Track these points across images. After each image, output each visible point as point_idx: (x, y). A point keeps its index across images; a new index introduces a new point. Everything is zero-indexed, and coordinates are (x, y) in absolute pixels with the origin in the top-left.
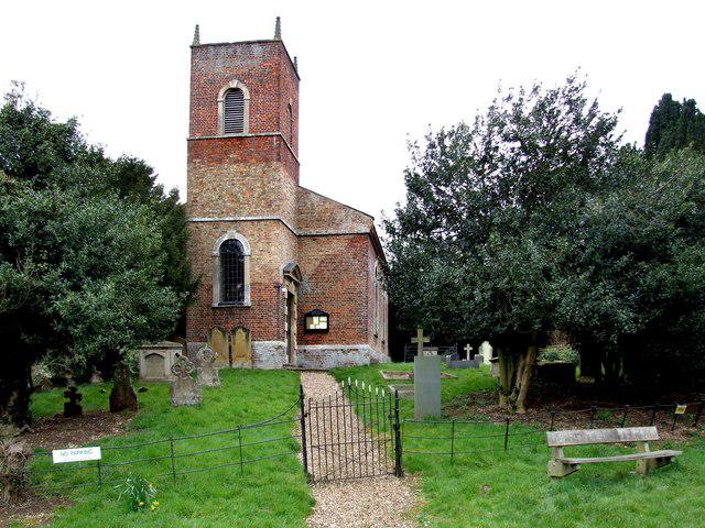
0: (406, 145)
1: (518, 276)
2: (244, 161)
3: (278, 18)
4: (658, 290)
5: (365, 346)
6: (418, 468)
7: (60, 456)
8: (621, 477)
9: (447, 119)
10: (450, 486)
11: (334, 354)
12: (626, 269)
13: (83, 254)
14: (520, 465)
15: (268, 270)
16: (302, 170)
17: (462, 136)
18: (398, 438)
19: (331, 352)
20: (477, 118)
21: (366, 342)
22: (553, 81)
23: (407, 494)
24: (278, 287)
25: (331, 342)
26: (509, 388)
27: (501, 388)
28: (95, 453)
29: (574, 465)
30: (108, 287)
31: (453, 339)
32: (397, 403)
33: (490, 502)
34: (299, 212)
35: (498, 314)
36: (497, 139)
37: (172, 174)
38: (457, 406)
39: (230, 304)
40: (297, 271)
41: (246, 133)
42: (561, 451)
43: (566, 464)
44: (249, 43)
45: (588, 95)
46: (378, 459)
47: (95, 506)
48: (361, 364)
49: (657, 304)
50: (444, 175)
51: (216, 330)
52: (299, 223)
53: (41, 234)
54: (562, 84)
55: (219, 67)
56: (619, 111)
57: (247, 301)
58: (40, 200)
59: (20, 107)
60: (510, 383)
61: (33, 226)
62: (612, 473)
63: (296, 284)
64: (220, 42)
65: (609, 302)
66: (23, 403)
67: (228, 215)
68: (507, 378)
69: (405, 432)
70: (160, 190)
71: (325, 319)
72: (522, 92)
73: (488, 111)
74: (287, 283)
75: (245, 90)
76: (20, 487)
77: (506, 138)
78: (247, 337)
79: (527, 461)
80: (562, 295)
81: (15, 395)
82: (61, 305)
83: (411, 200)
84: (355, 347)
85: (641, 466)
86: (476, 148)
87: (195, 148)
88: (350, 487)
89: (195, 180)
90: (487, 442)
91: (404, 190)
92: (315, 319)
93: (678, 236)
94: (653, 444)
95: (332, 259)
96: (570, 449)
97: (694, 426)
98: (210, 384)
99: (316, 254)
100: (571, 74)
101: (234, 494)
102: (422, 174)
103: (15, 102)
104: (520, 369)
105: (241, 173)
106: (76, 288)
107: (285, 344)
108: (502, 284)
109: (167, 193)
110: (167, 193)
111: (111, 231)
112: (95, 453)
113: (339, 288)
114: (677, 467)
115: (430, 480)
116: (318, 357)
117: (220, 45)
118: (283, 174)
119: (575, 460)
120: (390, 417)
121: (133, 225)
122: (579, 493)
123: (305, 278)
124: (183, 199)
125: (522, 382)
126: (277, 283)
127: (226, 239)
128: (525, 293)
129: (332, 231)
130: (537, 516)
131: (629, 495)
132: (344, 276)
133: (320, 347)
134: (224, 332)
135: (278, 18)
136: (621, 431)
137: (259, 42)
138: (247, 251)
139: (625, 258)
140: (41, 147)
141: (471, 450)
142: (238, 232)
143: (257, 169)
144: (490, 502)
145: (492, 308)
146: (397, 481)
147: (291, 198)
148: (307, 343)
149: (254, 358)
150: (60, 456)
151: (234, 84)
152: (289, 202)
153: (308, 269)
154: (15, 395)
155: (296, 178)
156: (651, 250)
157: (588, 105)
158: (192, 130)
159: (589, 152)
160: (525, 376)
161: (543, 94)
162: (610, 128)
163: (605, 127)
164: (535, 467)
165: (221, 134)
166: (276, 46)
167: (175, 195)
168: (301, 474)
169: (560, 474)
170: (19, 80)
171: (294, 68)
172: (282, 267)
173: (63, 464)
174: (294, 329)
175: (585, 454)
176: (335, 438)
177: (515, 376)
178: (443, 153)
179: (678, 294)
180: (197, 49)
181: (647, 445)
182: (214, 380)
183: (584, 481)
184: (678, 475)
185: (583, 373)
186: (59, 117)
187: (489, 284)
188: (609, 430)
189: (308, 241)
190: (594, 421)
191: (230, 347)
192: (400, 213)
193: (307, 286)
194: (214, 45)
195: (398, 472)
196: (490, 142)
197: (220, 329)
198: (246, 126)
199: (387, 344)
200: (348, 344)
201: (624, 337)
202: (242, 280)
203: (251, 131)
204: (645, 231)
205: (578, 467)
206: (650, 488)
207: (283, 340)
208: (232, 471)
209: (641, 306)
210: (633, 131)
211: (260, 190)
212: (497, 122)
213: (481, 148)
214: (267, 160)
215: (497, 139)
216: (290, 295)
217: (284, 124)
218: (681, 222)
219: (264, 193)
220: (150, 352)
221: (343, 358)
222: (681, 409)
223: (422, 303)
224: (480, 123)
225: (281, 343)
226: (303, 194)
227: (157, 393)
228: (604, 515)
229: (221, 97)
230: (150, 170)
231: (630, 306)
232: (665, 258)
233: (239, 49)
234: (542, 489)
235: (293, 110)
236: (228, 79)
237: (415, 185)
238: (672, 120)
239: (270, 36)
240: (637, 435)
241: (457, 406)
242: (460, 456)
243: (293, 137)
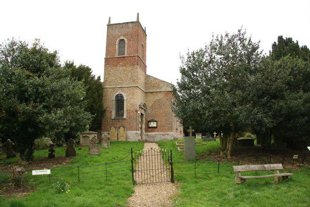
0: (179, 57)
1: (223, 106)
2: (125, 65)
3: (138, 14)
4: (280, 111)
5: (171, 133)
6: (180, 179)
7: (34, 173)
8: (267, 184)
9: (195, 47)
10: (193, 187)
11: (159, 136)
12: (267, 102)
13: (52, 100)
14: (224, 178)
15: (133, 105)
16: (147, 68)
17: (201, 54)
18: (172, 168)
19: (158, 135)
20: (206, 47)
22: (233, 32)
23: (174, 189)
26: (224, 148)
27: (221, 149)
28: (48, 172)
29: (245, 179)
30: (60, 112)
31: (207, 132)
32: (171, 155)
33: (206, 193)
34: (146, 84)
35: (216, 120)
36: (214, 54)
37: (98, 71)
38: (203, 156)
39: (119, 118)
40: (145, 105)
41: (126, 55)
42: (240, 174)
43: (242, 179)
44: (127, 23)
45: (246, 36)
46: (166, 175)
47: (44, 191)
48: (170, 139)
49: (281, 116)
50: (193, 69)
52: (146, 87)
53: (38, 93)
54: (237, 33)
55: (116, 32)
56: (259, 42)
57: (125, 116)
58: (37, 80)
59: (38, 48)
60: (224, 147)
61: (35, 90)
62: (263, 182)
65: (259, 115)
66: (31, 152)
68: (223, 144)
69: (175, 166)
70: (93, 77)
71: (156, 123)
72: (222, 37)
73: (210, 43)
74: (141, 110)
75: (126, 40)
76: (20, 184)
77: (218, 54)
79: (228, 177)
80: (241, 113)
81: (27, 150)
82: (41, 118)
83: (183, 78)
84: (168, 133)
85: (277, 179)
86: (206, 58)
87: (107, 61)
88: (151, 186)
89: (107, 73)
90: (212, 169)
91: (181, 74)
92: (152, 123)
93: (287, 89)
94: (281, 171)
95: (158, 101)
96: (243, 173)
97: (303, 163)
98: (107, 147)
99: (152, 99)
100: (240, 28)
101: (101, 188)
102: (186, 69)
103: (36, 46)
104: (228, 141)
106: (49, 112)
107: (139, 132)
108: (217, 108)
109: (96, 78)
110: (96, 78)
111: (65, 91)
112: (48, 172)
114: (291, 180)
115: (185, 184)
116: (153, 137)
117: (117, 24)
118: (139, 70)
119: (245, 177)
120: (168, 160)
121: (80, 90)
122: (245, 190)
123: (148, 108)
124: (102, 80)
125: (229, 146)
128: (226, 112)
129: (158, 90)
130: (224, 200)
131: (268, 192)
133: (154, 133)
135: (138, 14)
136: (266, 166)
137: (131, 22)
138: (125, 99)
139: (266, 98)
140: (42, 62)
141: (204, 172)
143: (129, 68)
144: (206, 193)
145: (214, 118)
146: (171, 184)
147: (143, 78)
148: (149, 132)
149: (127, 137)
150: (34, 173)
151: (122, 38)
152: (141, 81)
153: (149, 105)
154: (27, 150)
155: (145, 71)
156: (276, 95)
157: (248, 40)
158: (107, 54)
159: (249, 59)
160: (230, 144)
161: (230, 37)
162: (257, 48)
163: (255, 49)
164: (231, 179)
165: (117, 56)
166: (137, 24)
167: (99, 78)
168: (131, 181)
169: (240, 182)
170: (38, 39)
171: (144, 31)
172: (138, 104)
173: (279, 163)
174: (144, 126)
175: (253, 174)
176: (151, 167)
177: (226, 144)
178: (194, 60)
179: (289, 112)
180: (109, 26)
181: (278, 172)
182: (108, 146)
183: (249, 185)
184: (291, 183)
185: (258, 142)
186: (51, 51)
187: (212, 109)
188: (261, 165)
189: (150, 94)
190: (256, 162)
192: (178, 83)
193: (149, 111)
194: (115, 24)
195: (172, 181)
196: (212, 56)
198: (126, 53)
199: (182, 132)
201: (267, 128)
202: (123, 109)
204: (273, 87)
205: (247, 180)
206: (278, 189)
208: (103, 180)
209: (274, 117)
210: (265, 49)
212: (213, 48)
213: (208, 58)
215: (214, 54)
216: (142, 114)
217: (140, 51)
218: (288, 83)
220: (84, 135)
221: (163, 137)
222: (295, 157)
223: (187, 117)
224: (207, 49)
225: (137, 132)
226: (148, 77)
227: (85, 150)
228: (255, 200)
229: (117, 43)
230: (90, 70)
231: (270, 117)
232: (283, 98)
233: (124, 25)
234: (231, 189)
235: (144, 47)
237: (183, 72)
238: (284, 47)
239: (135, 20)
240: (273, 167)
241: (203, 156)
242: (199, 175)
243: (144, 56)
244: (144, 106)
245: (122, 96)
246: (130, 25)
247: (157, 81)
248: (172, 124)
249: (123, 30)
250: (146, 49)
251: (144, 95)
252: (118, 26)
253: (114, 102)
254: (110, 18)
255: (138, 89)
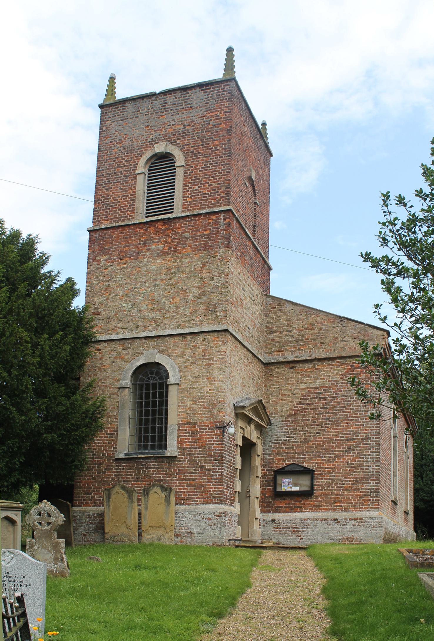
5: (375, 514)
11: (322, 526)
16: (273, 275)
21: (377, 508)
24: (222, 427)
25: (318, 508)
39: (148, 453)
41: (177, 212)
44: (185, 89)
51: (117, 489)
63: (259, 427)
64: (324, 310)
67: (146, 328)
74: (241, 423)
75: (177, 153)
78: (167, 500)
84: (359, 514)
105: (168, 269)
107: (236, 509)
113: (332, 434)
116: (295, 530)
117: (142, 98)
123: (276, 420)
126: (222, 422)
127: (141, 362)
129: (320, 354)
132: (340, 417)
133: (298, 516)
134: (130, 493)
135: (230, 51)
138: (172, 379)
142: (162, 352)
147: (256, 309)
148: (277, 510)
151: (160, 148)
158: (97, 216)
165: (140, 218)
172: (231, 401)
174: (256, 490)
191: (140, 514)
197: (123, 488)
199: (411, 516)
200: (346, 510)
203: (184, 210)
207: (232, 504)
211: (196, 292)
214: (208, 247)
219: (203, 294)
229: (142, 167)
236: (152, 143)
239: (219, 75)
244: (255, 410)
245: (125, 453)
246: (198, 96)
247: (313, 319)
248: (378, 482)
249: (167, 118)
250: (267, 203)
251: (257, 370)
252: (146, 104)
253: (127, 396)
254: (112, 79)
255: (230, 345)
